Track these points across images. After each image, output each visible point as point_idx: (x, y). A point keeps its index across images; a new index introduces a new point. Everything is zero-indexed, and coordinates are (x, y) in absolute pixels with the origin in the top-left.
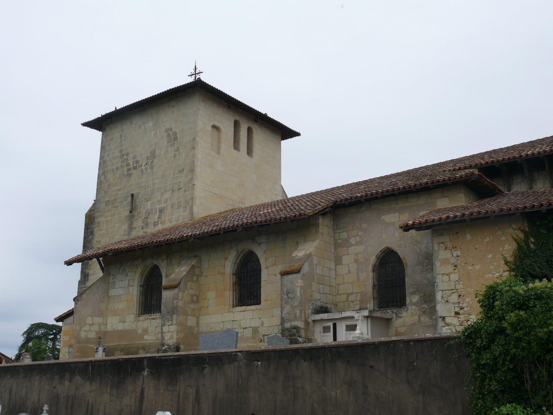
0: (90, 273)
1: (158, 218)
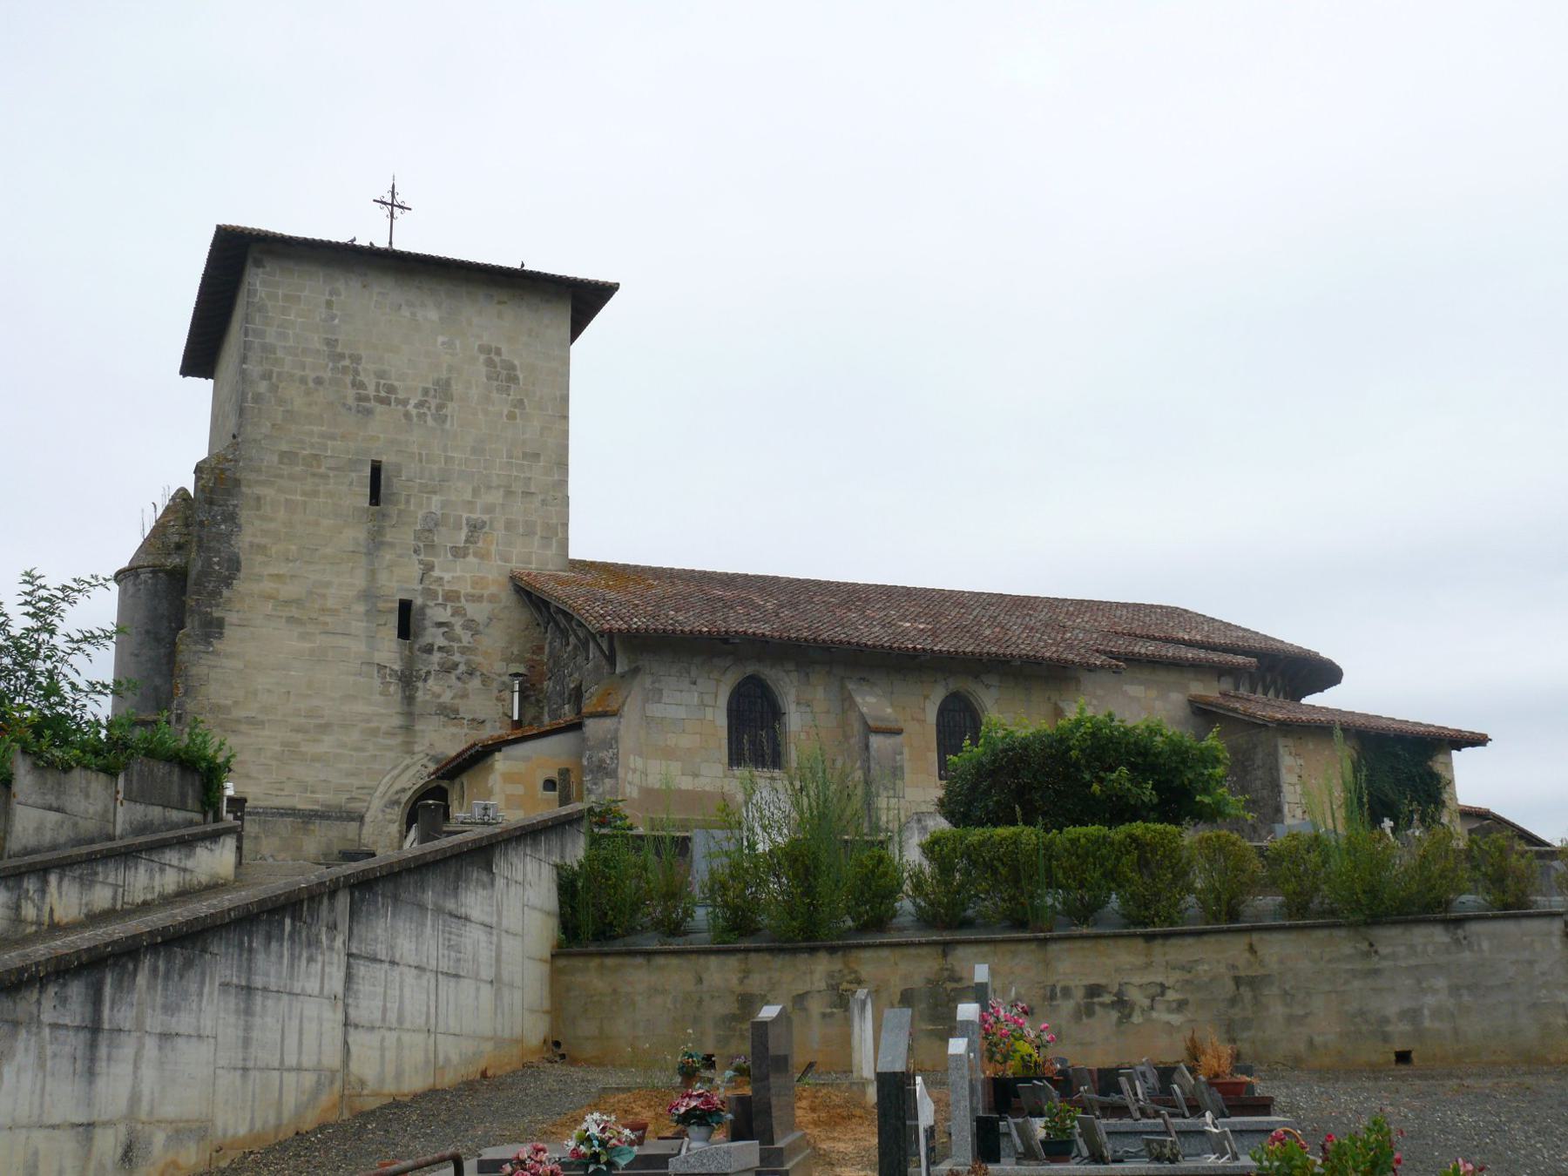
1: (467, 541)
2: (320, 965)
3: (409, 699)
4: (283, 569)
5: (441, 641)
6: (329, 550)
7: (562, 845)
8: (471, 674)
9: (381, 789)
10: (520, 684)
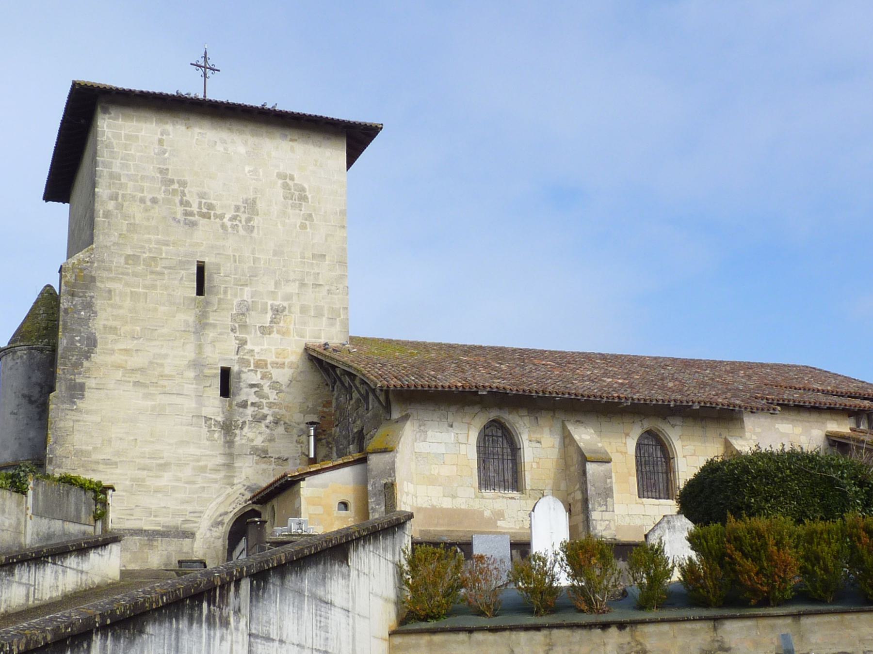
0: (87, 384)
1: (271, 322)
2: (229, 643)
3: (230, 443)
4: (131, 344)
5: (253, 399)
6: (165, 331)
7: (393, 544)
8: (277, 423)
9: (208, 512)
10: (315, 430)
